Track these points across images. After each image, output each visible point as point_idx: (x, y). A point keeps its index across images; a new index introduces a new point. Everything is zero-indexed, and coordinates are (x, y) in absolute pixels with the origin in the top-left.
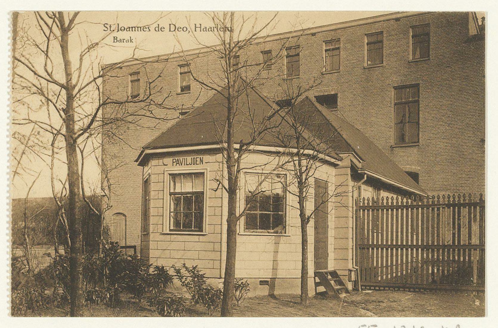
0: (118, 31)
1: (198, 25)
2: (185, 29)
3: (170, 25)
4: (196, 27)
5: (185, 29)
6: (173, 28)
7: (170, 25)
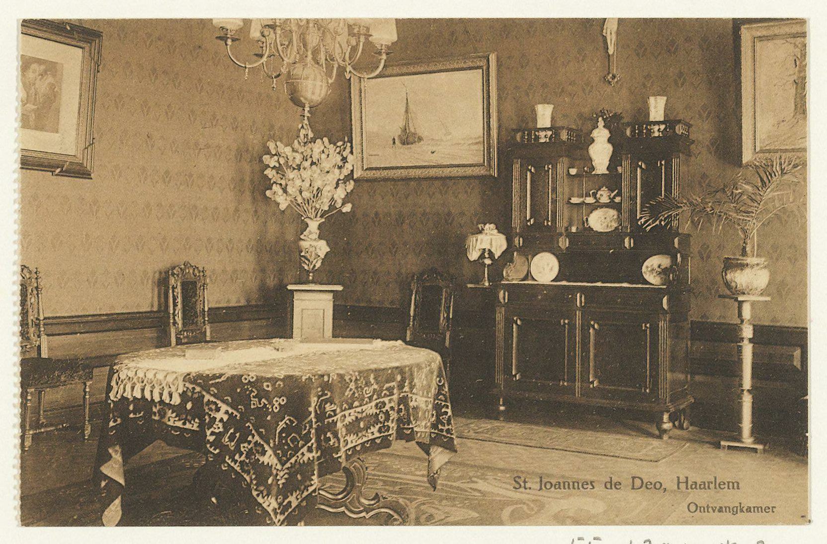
1: (682, 479)
2: (658, 486)
3: (634, 478)
4: (679, 483)
5: (658, 486)
6: (638, 483)
7: (634, 478)
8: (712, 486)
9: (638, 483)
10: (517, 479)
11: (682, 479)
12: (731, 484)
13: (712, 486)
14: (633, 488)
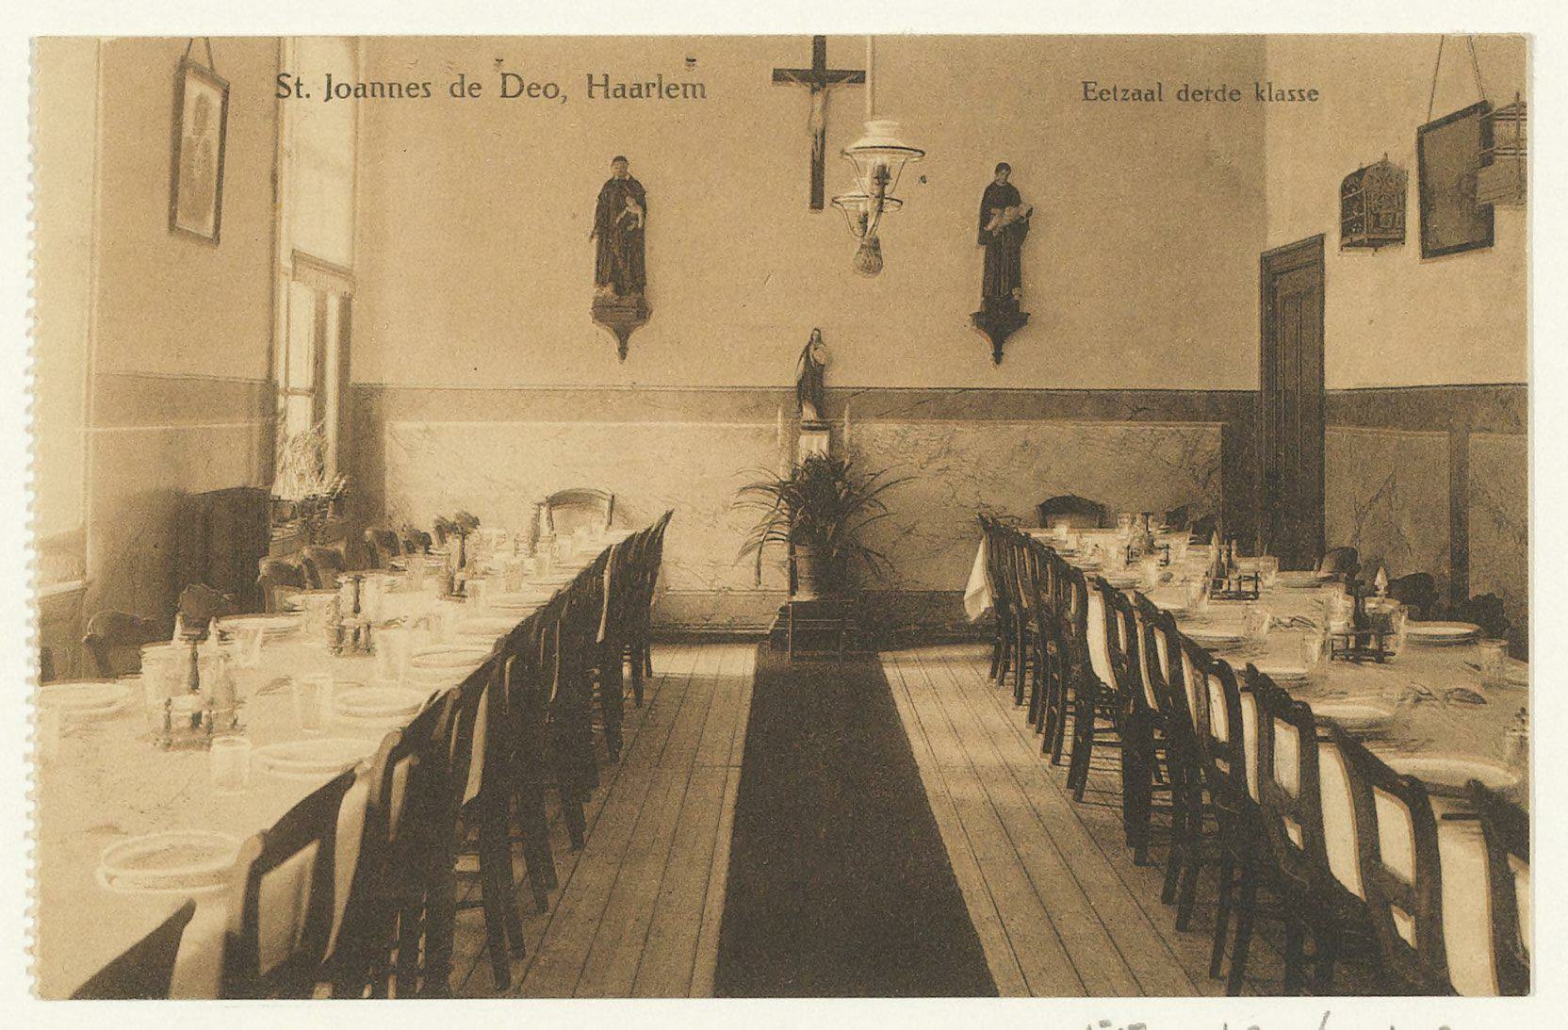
0: (329, 97)
1: (598, 79)
2: (551, 91)
5: (551, 91)
8: (654, 91)
9: (513, 85)
11: (598, 79)
12: (689, 89)
13: (654, 91)
14: (504, 95)
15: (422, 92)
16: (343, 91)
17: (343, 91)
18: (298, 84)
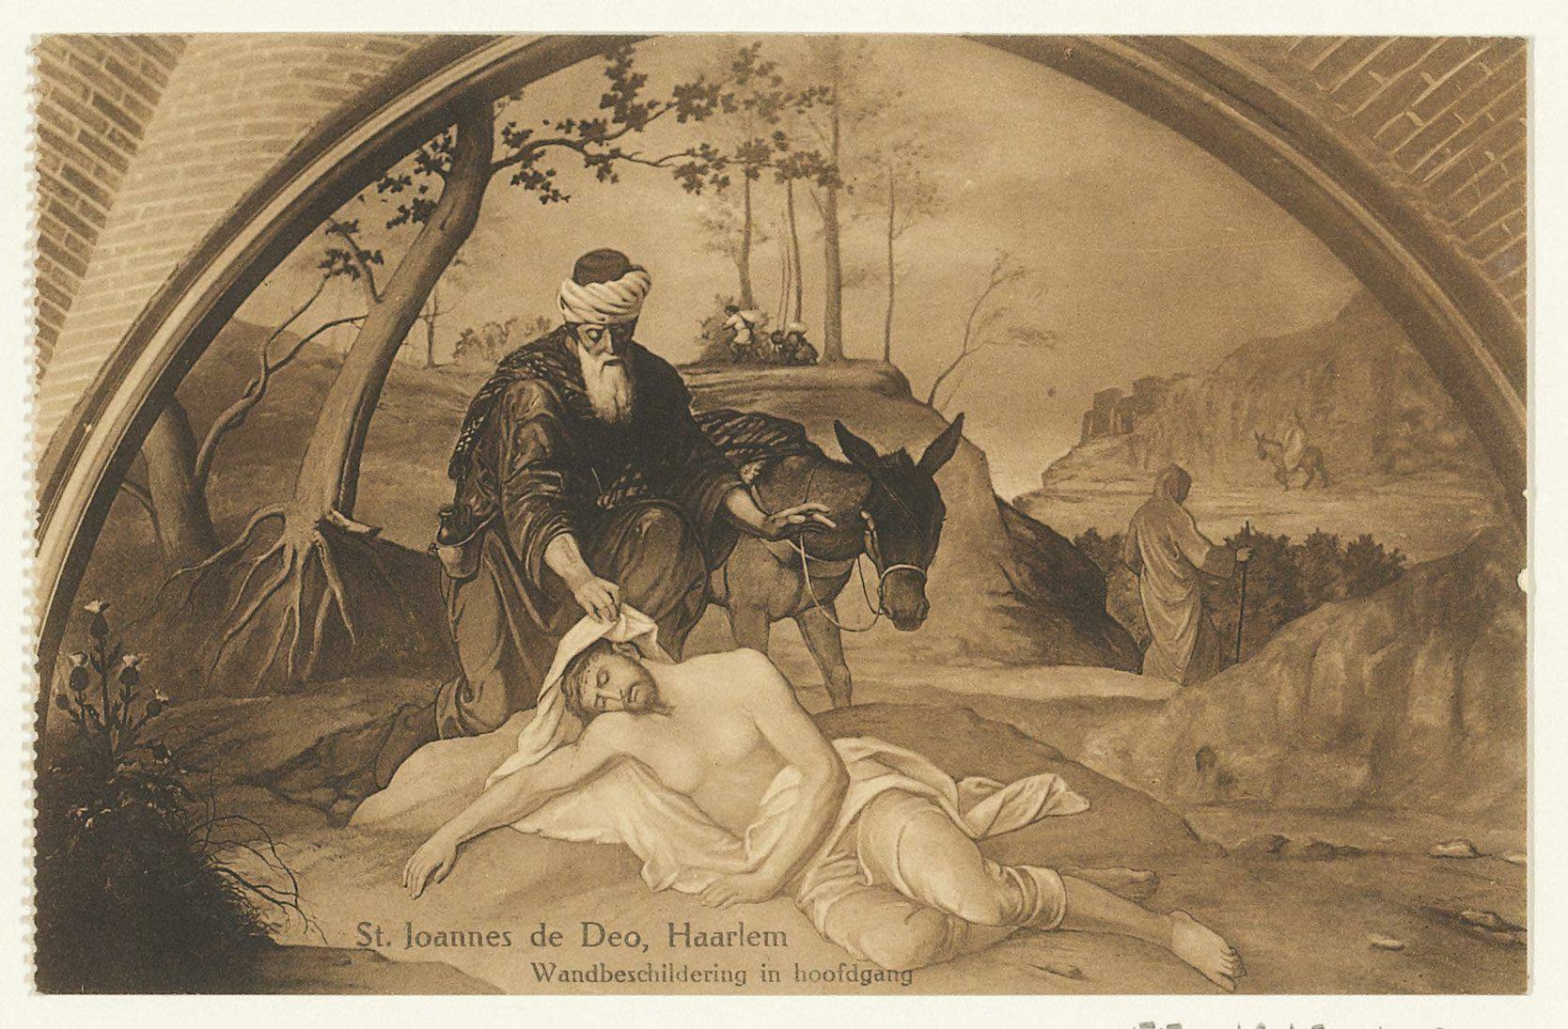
1: (679, 928)
3: (585, 924)
6: (594, 936)
7: (585, 924)
10: (364, 928)
11: (679, 928)
12: (770, 937)
13: (735, 940)
15: (502, 941)
16: (423, 940)
17: (423, 940)
18: (379, 932)
